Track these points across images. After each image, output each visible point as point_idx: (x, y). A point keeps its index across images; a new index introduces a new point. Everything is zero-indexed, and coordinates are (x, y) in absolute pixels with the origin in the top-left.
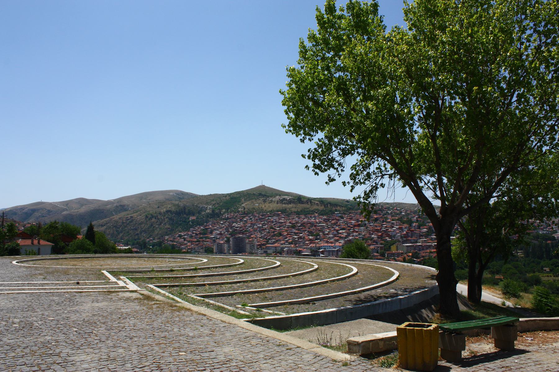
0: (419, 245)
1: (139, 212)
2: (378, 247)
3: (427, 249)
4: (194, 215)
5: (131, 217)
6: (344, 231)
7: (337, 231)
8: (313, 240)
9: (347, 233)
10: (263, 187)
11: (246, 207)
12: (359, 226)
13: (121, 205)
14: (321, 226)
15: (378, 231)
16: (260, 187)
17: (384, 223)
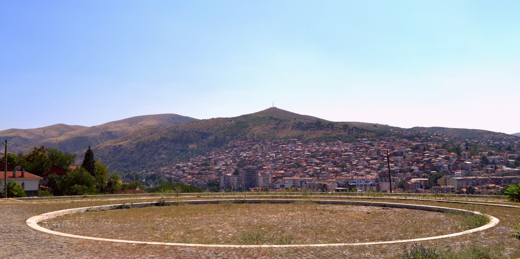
0: (473, 179)
1: (129, 140)
2: (421, 181)
3: (483, 183)
4: (192, 142)
5: (119, 146)
6: (376, 161)
7: (368, 161)
8: (339, 172)
9: (380, 163)
10: (274, 110)
11: (255, 134)
12: (395, 154)
13: (107, 132)
14: (347, 155)
15: (418, 162)
16: (271, 109)
17: (426, 152)
